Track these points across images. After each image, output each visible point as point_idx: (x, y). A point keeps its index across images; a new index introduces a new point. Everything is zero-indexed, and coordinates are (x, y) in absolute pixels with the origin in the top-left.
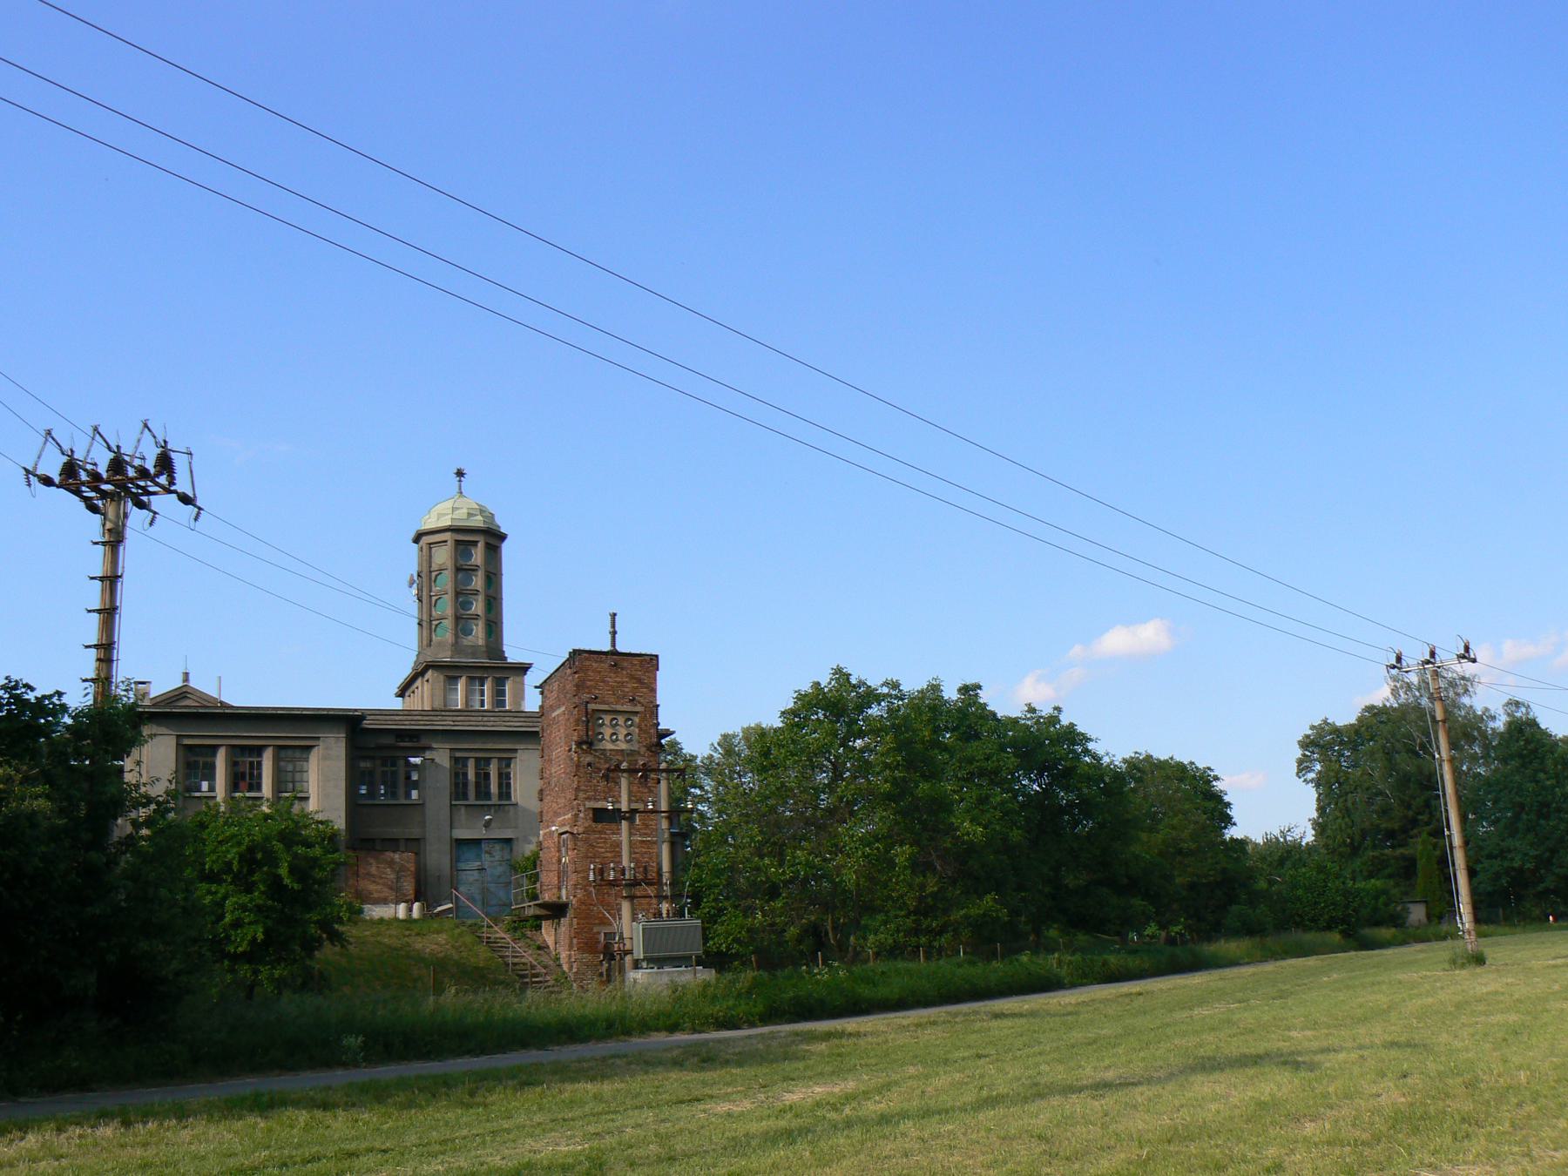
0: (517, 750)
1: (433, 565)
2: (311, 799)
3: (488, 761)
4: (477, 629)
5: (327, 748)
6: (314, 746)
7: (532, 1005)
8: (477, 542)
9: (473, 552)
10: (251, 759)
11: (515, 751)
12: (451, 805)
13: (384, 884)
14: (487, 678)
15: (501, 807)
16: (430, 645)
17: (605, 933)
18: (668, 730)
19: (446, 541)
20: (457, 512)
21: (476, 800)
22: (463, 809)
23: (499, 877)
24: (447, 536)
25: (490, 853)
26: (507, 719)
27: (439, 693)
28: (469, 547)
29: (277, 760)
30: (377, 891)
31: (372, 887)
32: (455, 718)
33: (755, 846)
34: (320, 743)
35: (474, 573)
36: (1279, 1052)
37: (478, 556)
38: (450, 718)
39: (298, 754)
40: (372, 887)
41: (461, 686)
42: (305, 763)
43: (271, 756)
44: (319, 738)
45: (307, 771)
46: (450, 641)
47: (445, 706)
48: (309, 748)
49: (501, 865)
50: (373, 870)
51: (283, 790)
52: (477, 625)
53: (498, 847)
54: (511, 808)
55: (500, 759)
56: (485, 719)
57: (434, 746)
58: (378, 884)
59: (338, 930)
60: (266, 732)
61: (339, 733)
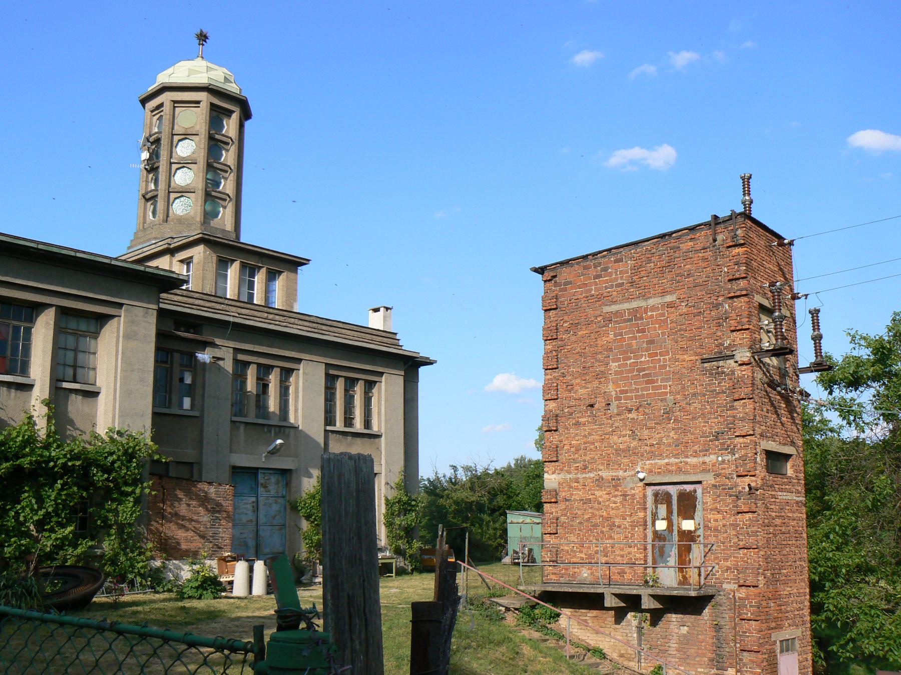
0: (302, 360)
1: (176, 127)
2: (101, 397)
3: (247, 364)
4: (224, 212)
5: (133, 322)
6: (113, 317)
7: (129, 656)
8: (232, 112)
9: (225, 123)
10: (16, 323)
11: (299, 361)
12: (326, 431)
13: (195, 531)
14: (260, 268)
15: (282, 429)
16: (167, 221)
17: (780, 641)
18: (428, 358)
19: (198, 102)
20: (211, 73)
21: (345, 426)
22: (242, 428)
23: (274, 518)
24: (202, 96)
25: (265, 487)
26: (293, 320)
27: (211, 275)
28: (221, 116)
29: (59, 331)
30: (186, 539)
31: (181, 534)
32: (240, 310)
33: (51, 459)
34: (123, 312)
35: (225, 146)
36: (203, 598)
37: (230, 127)
38: (234, 309)
39: (83, 326)
40: (181, 534)
41: (233, 272)
42: (93, 341)
43: (52, 323)
44: (120, 305)
45: (95, 353)
46: (198, 219)
47: (215, 293)
48: (103, 319)
49: (276, 502)
50: (183, 509)
51: (61, 378)
52: (225, 207)
53: (273, 479)
54: (292, 431)
55: (259, 365)
56: (271, 316)
57: (218, 341)
58: (187, 530)
59: (124, 601)
60: (79, 289)
61: (149, 303)
